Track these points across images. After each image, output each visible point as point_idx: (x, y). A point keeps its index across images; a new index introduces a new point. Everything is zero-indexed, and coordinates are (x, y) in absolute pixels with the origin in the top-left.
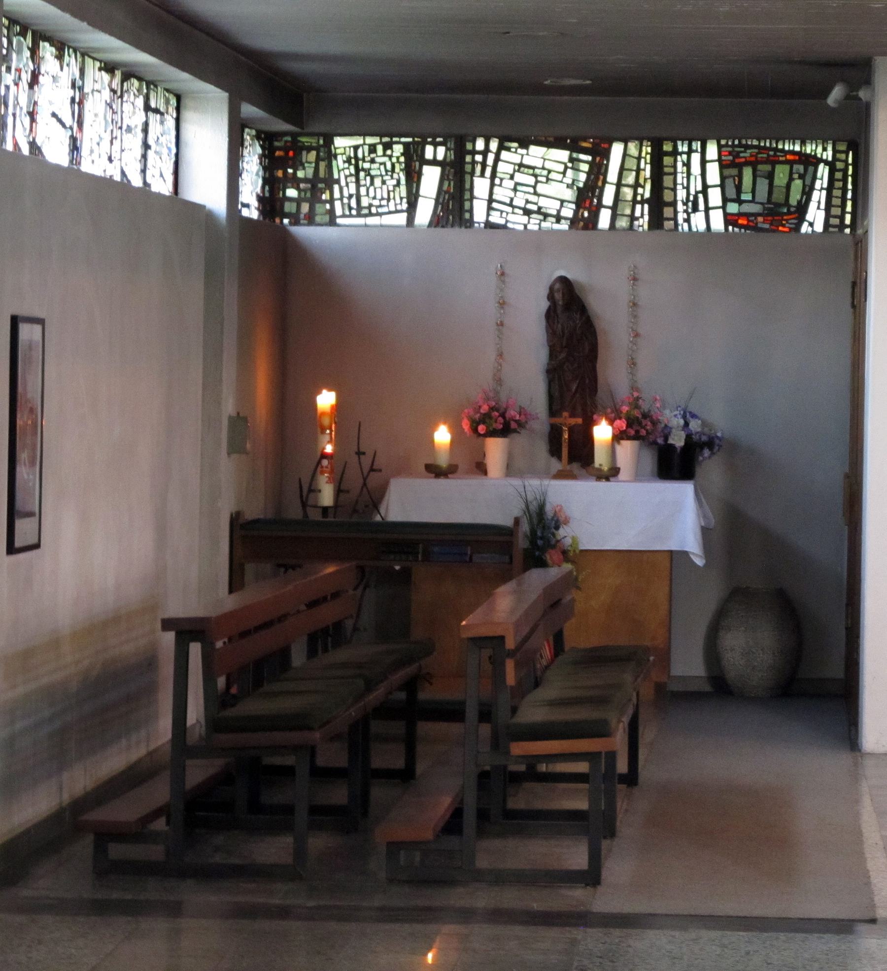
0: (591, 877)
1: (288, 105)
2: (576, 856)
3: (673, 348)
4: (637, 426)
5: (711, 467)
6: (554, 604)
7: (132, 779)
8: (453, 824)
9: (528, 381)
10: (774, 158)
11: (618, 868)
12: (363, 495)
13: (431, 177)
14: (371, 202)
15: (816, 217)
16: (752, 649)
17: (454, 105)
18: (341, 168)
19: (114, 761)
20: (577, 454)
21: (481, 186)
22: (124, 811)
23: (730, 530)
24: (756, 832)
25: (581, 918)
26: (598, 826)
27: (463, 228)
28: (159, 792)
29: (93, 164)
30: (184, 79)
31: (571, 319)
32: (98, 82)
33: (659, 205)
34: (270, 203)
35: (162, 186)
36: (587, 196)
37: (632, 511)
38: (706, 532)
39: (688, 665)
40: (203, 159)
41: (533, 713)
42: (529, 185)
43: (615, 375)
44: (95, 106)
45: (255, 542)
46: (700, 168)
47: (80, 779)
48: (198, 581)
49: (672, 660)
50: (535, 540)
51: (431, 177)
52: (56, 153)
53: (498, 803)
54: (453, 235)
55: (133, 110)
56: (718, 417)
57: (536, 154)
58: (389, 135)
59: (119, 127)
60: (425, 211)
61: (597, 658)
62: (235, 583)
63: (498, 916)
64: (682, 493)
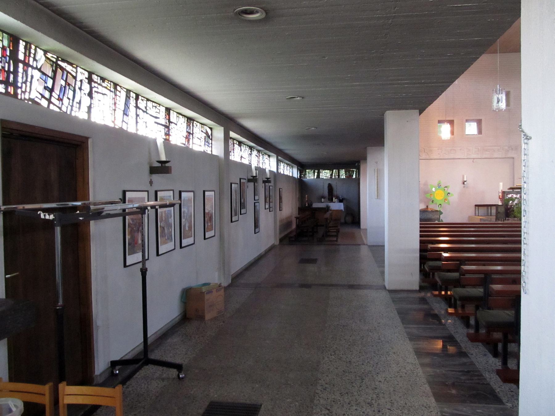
0: (337, 241)
1: (302, 167)
2: (335, 239)
3: (339, 190)
4: (337, 197)
5: (344, 201)
6: (331, 215)
7: (291, 232)
8: (323, 236)
9: (326, 193)
10: (350, 171)
11: (339, 240)
12: (310, 205)
13: (316, 174)
14: (310, 176)
15: (354, 177)
16: (349, 219)
17: (318, 166)
18: (307, 173)
19: (289, 231)
20: (331, 200)
21: (321, 174)
22: (292, 235)
23: (346, 207)
24: (352, 236)
25: (336, 245)
26: (337, 236)
27: (523, 247)
28: (294, 233)
29: (285, 173)
30: (293, 165)
31: (330, 187)
32: (285, 165)
33: (339, 176)
34: (300, 176)
35: (291, 175)
36: (331, 175)
37: (337, 206)
38: (344, 208)
39: (343, 221)
40: (294, 173)
41: (330, 225)
42: (325, 174)
43: (335, 193)
44: (285, 167)
45: (301, 209)
46: (343, 172)
47: (286, 233)
48: (295, 213)
49: (7, 364)
50: (327, 209)
51: (316, 174)
52: (282, 173)
53: (327, 235)
54: (318, 179)
55: (288, 167)
56: (345, 197)
57: (326, 171)
58: (312, 169)
59: (287, 170)
60: (315, 177)
61: (335, 220)
62: (299, 214)
63: (328, 245)
64: (342, 204)
